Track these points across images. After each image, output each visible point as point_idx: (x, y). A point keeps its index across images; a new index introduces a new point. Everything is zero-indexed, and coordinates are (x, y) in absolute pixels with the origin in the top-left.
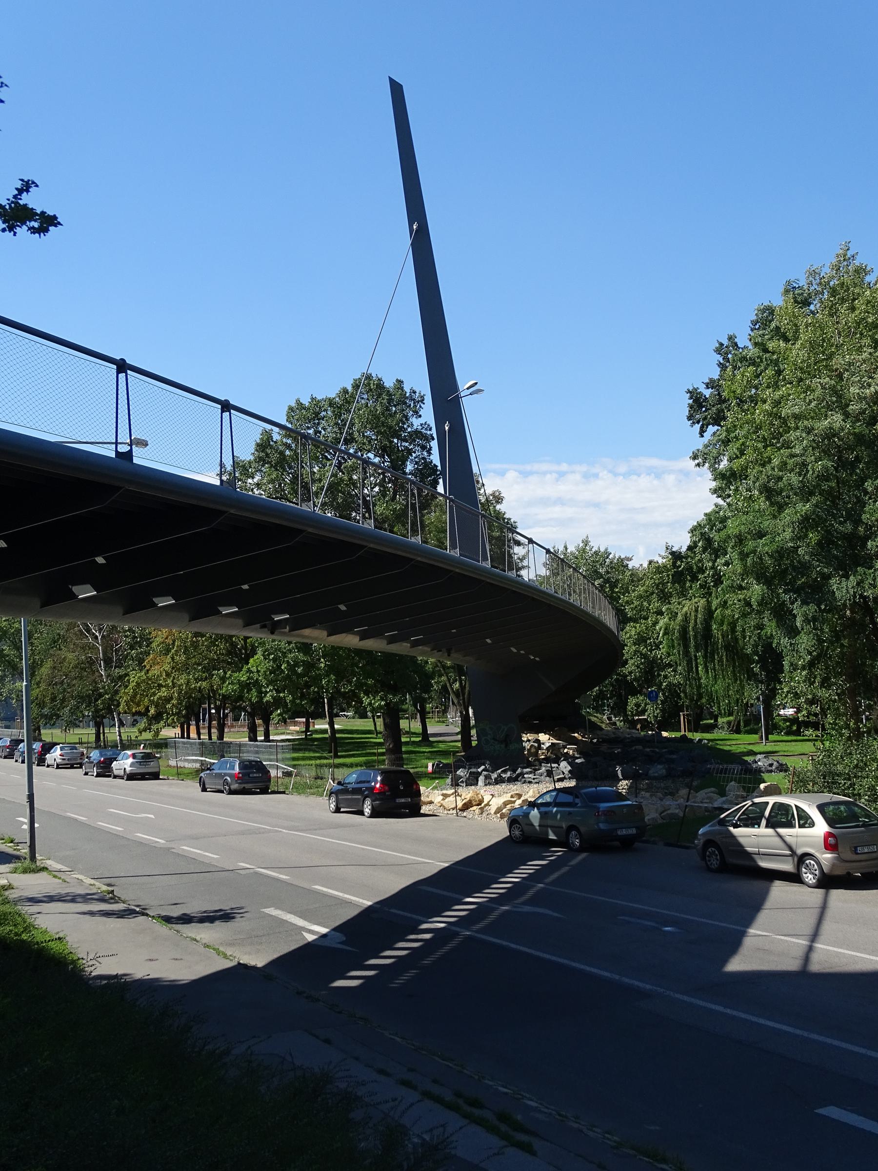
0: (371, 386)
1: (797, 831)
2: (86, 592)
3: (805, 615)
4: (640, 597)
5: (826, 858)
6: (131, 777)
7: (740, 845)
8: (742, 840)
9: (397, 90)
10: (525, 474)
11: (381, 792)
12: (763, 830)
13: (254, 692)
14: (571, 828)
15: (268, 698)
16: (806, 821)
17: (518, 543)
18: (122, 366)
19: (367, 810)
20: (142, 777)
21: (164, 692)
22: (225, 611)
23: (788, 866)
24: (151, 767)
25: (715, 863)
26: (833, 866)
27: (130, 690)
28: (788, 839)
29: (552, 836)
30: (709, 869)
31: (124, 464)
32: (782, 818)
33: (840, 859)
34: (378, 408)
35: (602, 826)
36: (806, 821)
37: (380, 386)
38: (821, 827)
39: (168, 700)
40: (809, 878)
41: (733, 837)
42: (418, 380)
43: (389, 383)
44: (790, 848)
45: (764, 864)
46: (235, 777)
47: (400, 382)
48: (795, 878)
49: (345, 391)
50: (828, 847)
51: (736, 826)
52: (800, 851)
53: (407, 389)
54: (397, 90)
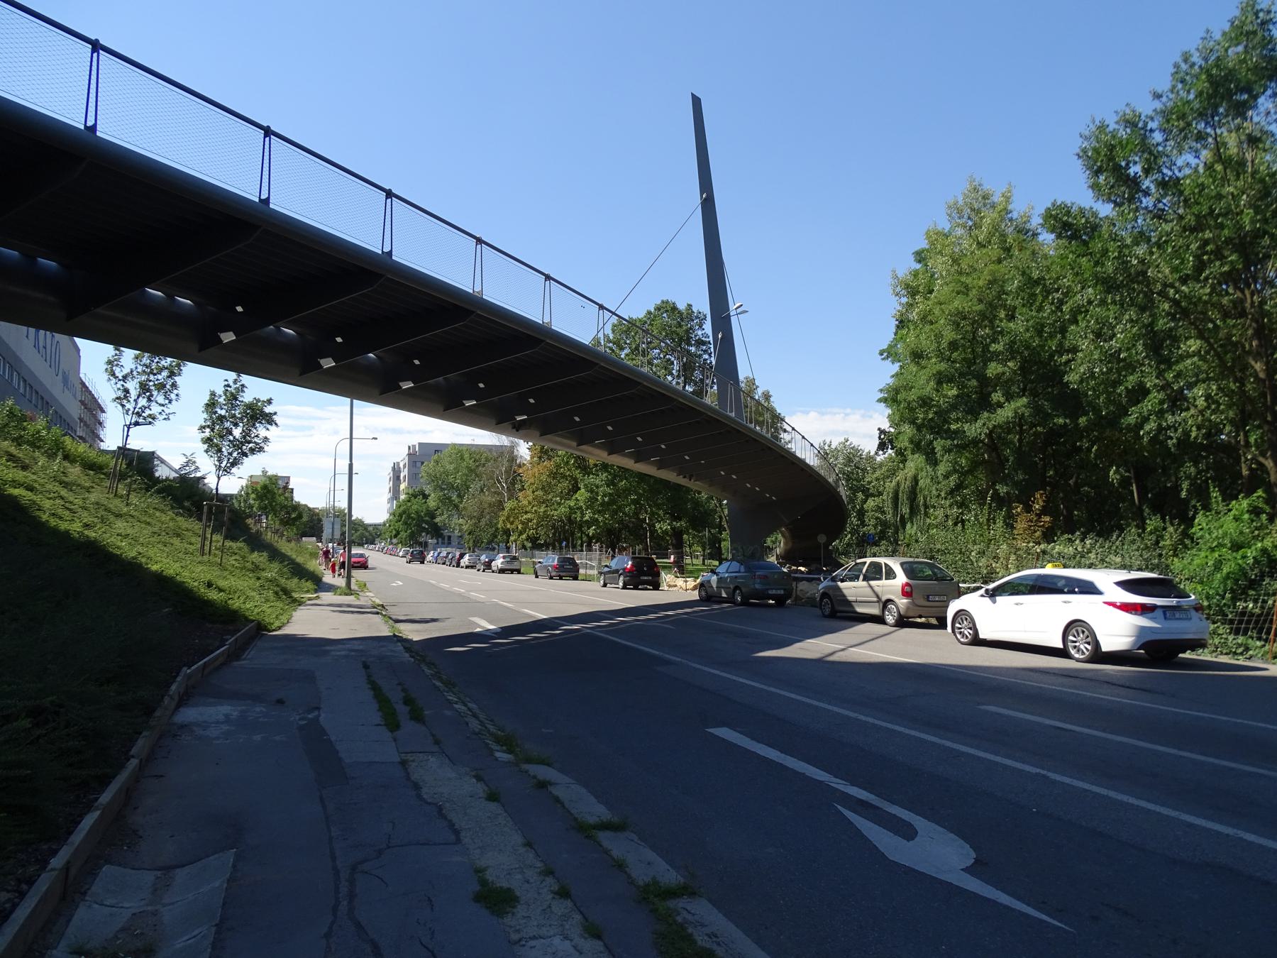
0: (668, 308)
1: (884, 582)
2: (328, 363)
3: (944, 447)
4: (877, 479)
5: (903, 602)
6: (502, 571)
7: (844, 596)
8: (846, 592)
9: (696, 102)
10: (823, 414)
11: (630, 571)
12: (861, 583)
13: (579, 514)
14: (736, 588)
15: (587, 518)
16: (890, 574)
17: (785, 431)
18: (268, 132)
19: (621, 584)
20: (512, 571)
21: (529, 516)
22: (468, 404)
23: (875, 611)
24: (515, 565)
25: (827, 611)
26: (908, 609)
27: (505, 513)
28: (876, 589)
29: (724, 595)
30: (825, 616)
31: (263, 206)
32: (876, 572)
33: (914, 603)
34: (672, 325)
35: (757, 586)
36: (890, 574)
37: (674, 308)
38: (901, 578)
39: (531, 520)
40: (890, 619)
41: (839, 589)
42: (702, 304)
43: (682, 306)
44: (878, 596)
45: (859, 610)
46: (555, 567)
47: (690, 306)
48: (879, 620)
49: (649, 313)
50: (905, 594)
51: (842, 581)
52: (884, 599)
53: (695, 310)
54: (696, 102)
